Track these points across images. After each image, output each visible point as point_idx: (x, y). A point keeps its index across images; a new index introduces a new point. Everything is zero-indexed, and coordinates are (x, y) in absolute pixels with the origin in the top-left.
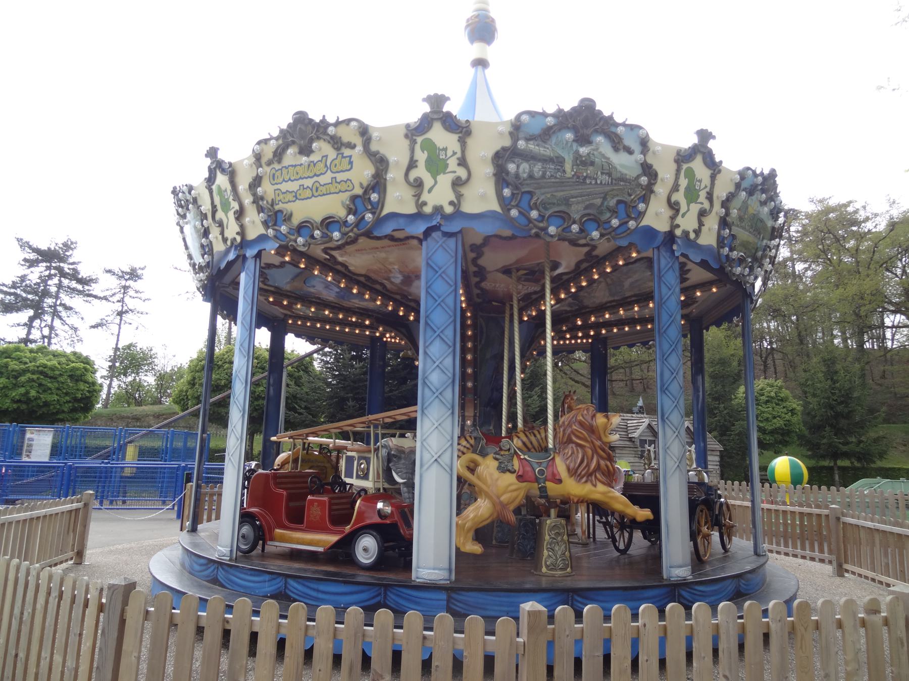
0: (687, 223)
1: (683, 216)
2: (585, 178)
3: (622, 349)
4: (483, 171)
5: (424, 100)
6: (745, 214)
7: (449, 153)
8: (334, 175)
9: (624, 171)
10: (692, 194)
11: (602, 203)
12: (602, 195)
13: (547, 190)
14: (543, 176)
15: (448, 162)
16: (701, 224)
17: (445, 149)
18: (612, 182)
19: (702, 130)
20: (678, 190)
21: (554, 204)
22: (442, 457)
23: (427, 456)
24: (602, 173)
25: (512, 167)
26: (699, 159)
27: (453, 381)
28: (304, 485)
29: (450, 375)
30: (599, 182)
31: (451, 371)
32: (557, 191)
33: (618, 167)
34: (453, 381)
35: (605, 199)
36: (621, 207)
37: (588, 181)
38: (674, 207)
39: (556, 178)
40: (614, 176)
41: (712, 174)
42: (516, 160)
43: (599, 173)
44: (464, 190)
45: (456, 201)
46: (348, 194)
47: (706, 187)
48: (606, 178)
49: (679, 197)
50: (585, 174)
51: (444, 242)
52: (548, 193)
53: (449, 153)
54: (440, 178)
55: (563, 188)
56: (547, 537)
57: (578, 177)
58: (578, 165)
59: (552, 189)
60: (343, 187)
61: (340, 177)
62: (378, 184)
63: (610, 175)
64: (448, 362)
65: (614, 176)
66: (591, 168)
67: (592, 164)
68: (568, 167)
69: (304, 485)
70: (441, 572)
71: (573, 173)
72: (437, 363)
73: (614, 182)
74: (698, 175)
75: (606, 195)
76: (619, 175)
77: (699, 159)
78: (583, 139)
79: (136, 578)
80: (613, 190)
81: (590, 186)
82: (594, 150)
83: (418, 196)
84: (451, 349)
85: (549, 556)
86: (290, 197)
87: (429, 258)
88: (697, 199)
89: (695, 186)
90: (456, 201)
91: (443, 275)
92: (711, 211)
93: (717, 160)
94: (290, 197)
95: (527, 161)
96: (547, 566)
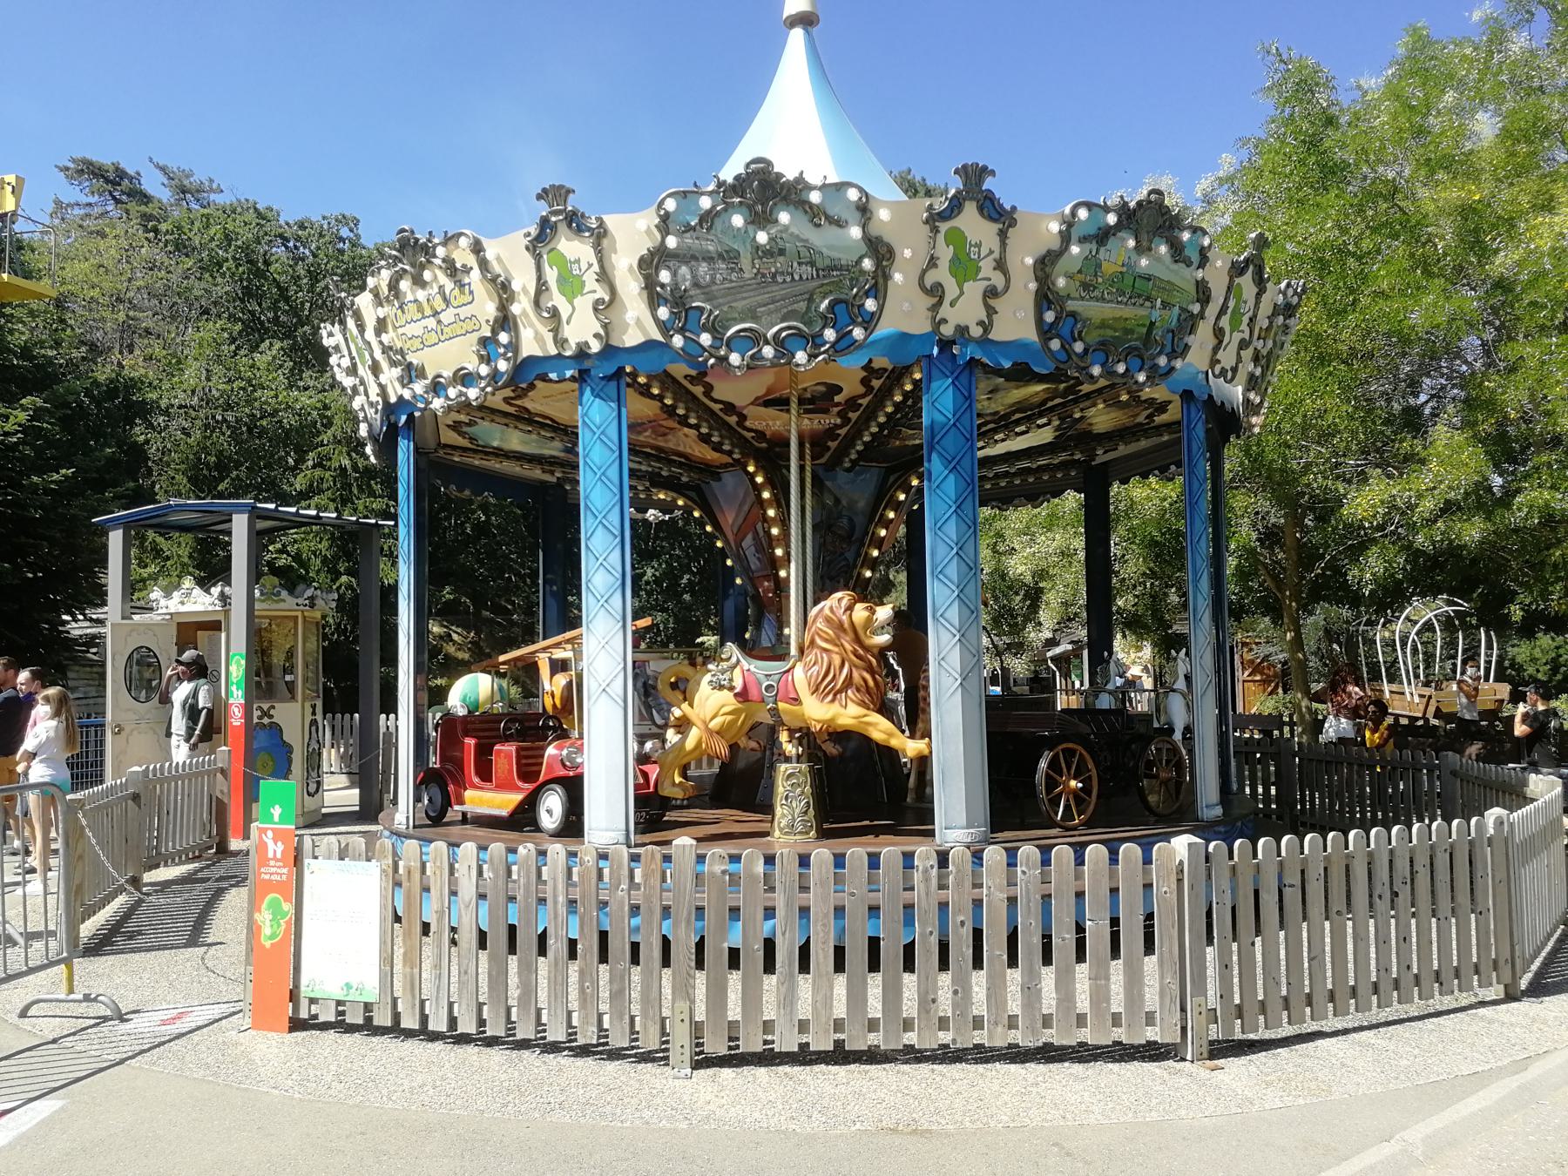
0: (964, 311)
1: (952, 305)
2: (774, 276)
3: (1152, 479)
4: (630, 287)
5: (539, 197)
6: (1096, 275)
7: (584, 266)
8: (456, 311)
9: (835, 255)
10: (964, 267)
11: (808, 308)
12: (807, 296)
13: (721, 301)
14: (713, 281)
15: (584, 278)
16: (991, 312)
17: (578, 261)
18: (818, 275)
19: (965, 167)
20: (935, 266)
21: (735, 319)
22: (611, 685)
23: (594, 686)
24: (799, 264)
25: (665, 276)
26: (970, 208)
27: (623, 584)
28: (493, 733)
29: (619, 576)
30: (797, 277)
31: (620, 569)
32: (736, 301)
33: (824, 250)
34: (623, 584)
35: (810, 300)
36: (840, 309)
37: (780, 279)
38: (937, 292)
39: (731, 281)
40: (820, 264)
41: (1001, 230)
42: (671, 264)
43: (795, 264)
44: (613, 315)
45: (602, 333)
46: (476, 336)
47: (991, 252)
48: (807, 271)
49: (942, 274)
50: (773, 270)
51: (601, 390)
52: (724, 304)
53: (584, 266)
54: (577, 301)
55: (744, 295)
56: (781, 789)
57: (764, 276)
58: (761, 258)
59: (729, 298)
60: (469, 326)
61: (464, 312)
62: (505, 321)
63: (812, 264)
64: (615, 557)
65: (820, 264)
66: (781, 259)
67: (782, 252)
68: (745, 262)
69: (493, 733)
70: (613, 834)
71: (755, 271)
72: (601, 560)
73: (821, 273)
74: (972, 237)
75: (812, 295)
76: (827, 262)
77: (970, 208)
78: (761, 219)
79: (460, 894)
80: (823, 285)
81: (784, 286)
82: (781, 231)
83: (556, 331)
84: (618, 539)
85: (784, 816)
86: (417, 344)
87: (586, 414)
88: (977, 274)
89: (969, 254)
90: (602, 333)
91: (602, 437)
92: (1007, 288)
93: (1008, 207)
94: (417, 344)
95: (687, 263)
96: (781, 830)
